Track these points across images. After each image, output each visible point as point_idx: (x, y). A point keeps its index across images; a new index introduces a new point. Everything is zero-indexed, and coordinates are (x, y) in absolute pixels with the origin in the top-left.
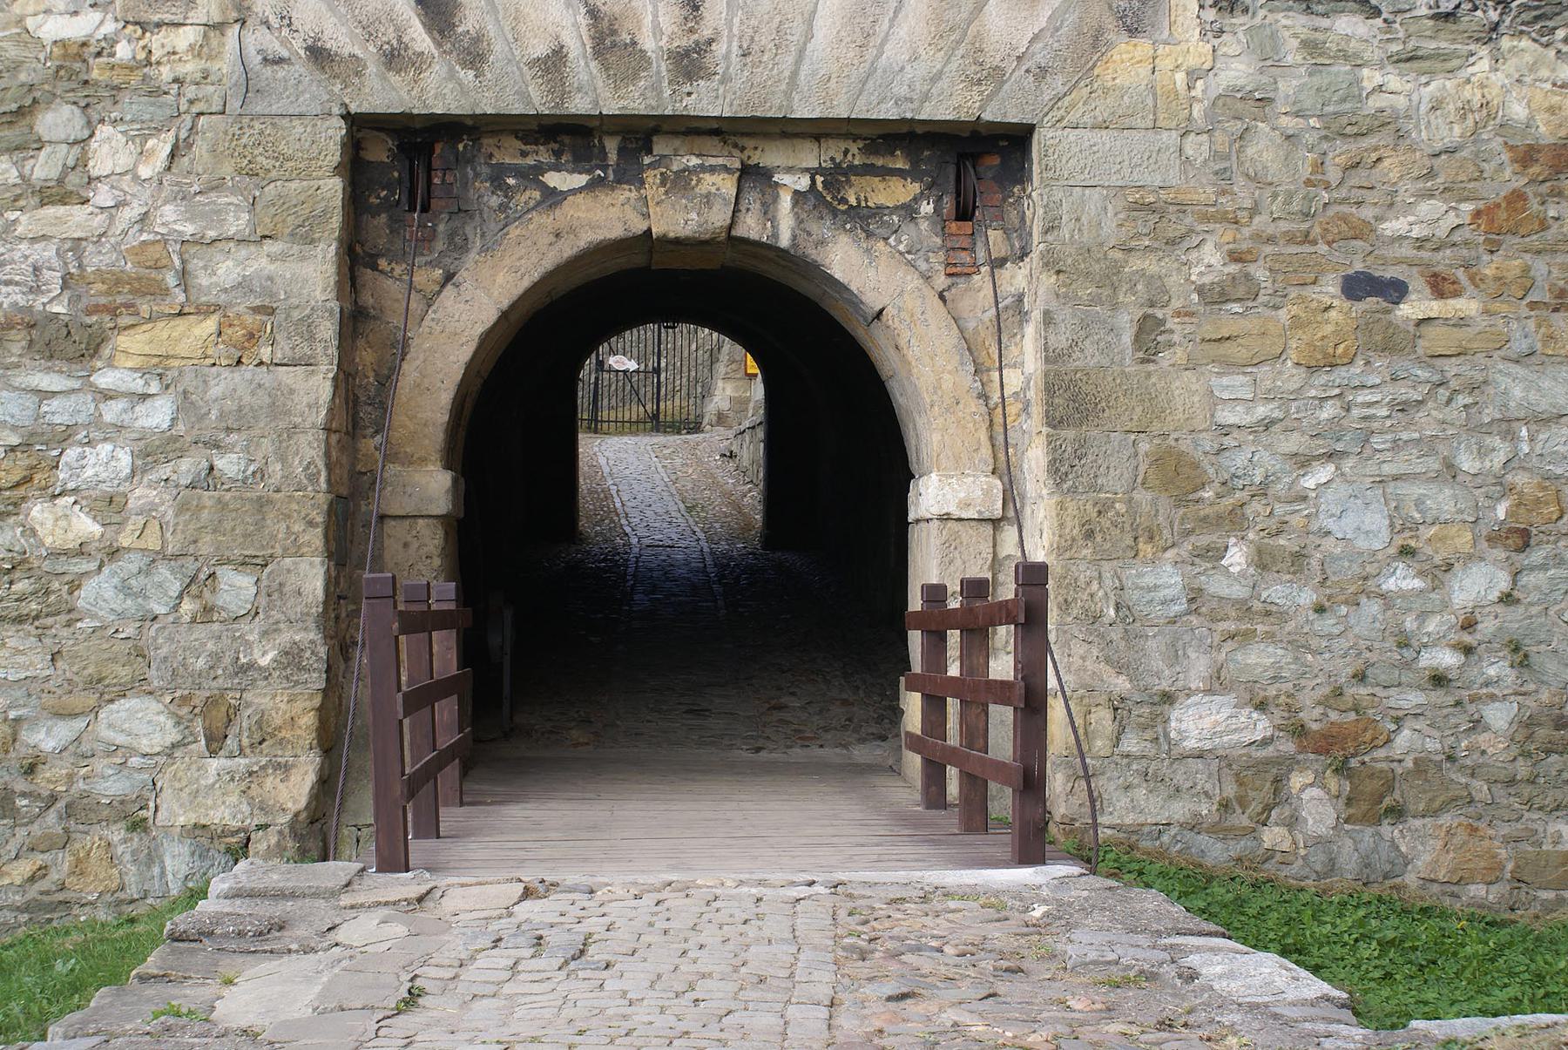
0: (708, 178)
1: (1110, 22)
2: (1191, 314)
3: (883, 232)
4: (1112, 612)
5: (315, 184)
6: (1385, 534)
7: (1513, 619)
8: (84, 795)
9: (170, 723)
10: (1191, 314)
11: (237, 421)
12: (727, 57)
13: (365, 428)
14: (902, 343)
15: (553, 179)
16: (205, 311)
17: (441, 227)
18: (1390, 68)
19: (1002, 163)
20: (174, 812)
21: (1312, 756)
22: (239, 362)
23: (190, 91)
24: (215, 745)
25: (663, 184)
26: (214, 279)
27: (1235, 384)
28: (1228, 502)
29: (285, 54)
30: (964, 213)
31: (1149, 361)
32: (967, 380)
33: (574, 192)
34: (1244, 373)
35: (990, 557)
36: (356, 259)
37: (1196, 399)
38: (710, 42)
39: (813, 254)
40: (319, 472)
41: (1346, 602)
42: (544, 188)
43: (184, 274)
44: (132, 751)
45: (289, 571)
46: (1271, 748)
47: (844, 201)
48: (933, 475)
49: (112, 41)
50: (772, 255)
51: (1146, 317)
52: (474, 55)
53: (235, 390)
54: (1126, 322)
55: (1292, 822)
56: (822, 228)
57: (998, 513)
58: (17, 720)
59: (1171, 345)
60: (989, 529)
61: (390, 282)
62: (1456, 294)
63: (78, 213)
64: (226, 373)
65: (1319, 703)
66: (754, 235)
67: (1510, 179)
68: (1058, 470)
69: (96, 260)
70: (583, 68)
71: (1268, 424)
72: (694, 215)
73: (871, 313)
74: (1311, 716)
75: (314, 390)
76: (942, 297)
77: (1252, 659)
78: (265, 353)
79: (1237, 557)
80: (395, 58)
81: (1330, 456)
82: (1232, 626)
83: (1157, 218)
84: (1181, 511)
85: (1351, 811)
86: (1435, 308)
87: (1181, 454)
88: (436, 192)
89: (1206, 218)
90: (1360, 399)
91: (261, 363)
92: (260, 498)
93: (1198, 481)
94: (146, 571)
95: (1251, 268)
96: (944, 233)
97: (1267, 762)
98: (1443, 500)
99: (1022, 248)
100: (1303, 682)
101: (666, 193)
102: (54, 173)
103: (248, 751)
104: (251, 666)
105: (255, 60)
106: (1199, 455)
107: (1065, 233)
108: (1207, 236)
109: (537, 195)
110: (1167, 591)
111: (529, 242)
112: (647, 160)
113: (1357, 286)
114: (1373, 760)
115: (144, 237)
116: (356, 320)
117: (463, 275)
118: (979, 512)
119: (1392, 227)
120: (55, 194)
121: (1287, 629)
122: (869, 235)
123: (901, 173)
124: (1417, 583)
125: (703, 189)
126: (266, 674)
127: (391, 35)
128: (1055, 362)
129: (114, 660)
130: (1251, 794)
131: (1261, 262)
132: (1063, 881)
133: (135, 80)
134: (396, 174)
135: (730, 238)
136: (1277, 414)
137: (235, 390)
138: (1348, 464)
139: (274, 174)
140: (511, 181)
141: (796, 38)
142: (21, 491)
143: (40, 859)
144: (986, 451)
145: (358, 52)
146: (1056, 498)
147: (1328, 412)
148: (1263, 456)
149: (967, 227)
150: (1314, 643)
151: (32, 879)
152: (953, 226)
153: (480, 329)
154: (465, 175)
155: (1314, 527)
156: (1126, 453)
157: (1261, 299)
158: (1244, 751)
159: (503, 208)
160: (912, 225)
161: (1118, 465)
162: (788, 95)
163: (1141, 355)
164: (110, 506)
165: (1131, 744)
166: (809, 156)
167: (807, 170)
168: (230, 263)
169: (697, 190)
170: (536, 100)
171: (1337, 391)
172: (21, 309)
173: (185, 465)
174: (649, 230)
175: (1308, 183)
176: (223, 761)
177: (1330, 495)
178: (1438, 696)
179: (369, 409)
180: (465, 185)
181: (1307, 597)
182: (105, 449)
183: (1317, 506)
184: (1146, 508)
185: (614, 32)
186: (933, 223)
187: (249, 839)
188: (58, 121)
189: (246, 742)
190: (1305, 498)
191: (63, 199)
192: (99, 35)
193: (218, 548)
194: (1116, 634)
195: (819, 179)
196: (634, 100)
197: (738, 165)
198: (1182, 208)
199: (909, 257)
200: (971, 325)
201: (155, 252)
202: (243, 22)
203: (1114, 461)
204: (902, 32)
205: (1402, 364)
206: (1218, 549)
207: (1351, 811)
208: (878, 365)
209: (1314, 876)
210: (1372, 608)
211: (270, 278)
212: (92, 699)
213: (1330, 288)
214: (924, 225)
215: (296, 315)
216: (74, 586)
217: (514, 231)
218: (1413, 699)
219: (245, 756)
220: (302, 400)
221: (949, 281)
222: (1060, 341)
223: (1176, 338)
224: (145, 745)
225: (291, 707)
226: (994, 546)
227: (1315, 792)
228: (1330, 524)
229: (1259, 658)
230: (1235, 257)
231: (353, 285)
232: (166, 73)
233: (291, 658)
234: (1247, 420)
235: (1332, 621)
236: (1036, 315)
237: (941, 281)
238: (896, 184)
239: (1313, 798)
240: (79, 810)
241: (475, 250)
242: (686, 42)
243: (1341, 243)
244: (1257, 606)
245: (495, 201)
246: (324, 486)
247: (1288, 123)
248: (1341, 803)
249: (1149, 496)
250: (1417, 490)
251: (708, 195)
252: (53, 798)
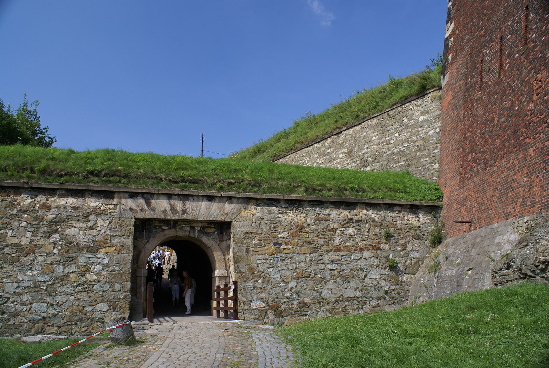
7: (297, 289)
8: (94, 318)
15: (163, 227)
23: (112, 214)
27: (260, 257)
36: (135, 239)
43: (111, 240)
44: (101, 311)
54: (245, 248)
55: (268, 318)
63: (95, 231)
67: (295, 229)
69: (97, 238)
70: (169, 212)
74: (270, 304)
75: (129, 258)
78: (122, 252)
79: (260, 281)
80: (142, 210)
81: (272, 267)
83: (249, 235)
86: (286, 247)
98: (288, 273)
105: (122, 210)
116: (135, 247)
119: (281, 235)
120: (92, 228)
126: (122, 299)
133: (104, 212)
135: (189, 236)
143: (87, 328)
151: (86, 331)
164: (99, 274)
165: (246, 308)
166: (200, 225)
170: (162, 216)
173: (110, 268)
178: (287, 300)
181: (269, 287)
188: (92, 218)
191: (93, 229)
196: (176, 217)
198: (252, 233)
205: (281, 254)
210: (279, 288)
213: (272, 244)
216: (93, 286)
217: (158, 235)
220: (128, 259)
224: (103, 310)
225: (125, 304)
229: (263, 295)
232: (109, 211)
233: (126, 297)
237: (218, 243)
240: (93, 320)
247: (266, 222)
252: (89, 318)
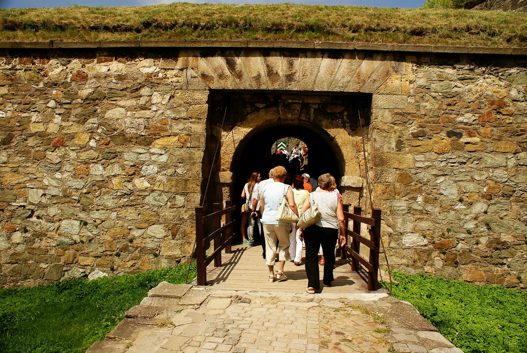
0: (294, 105)
1: (391, 70)
6: (457, 195)
7: (487, 217)
9: (164, 231)
10: (410, 140)
11: (182, 161)
12: (299, 76)
16: (175, 135)
17: (232, 116)
18: (459, 81)
20: (165, 252)
29: (196, 76)
38: (295, 73)
49: (158, 72)
52: (239, 76)
58: (130, 229)
59: (404, 147)
62: (475, 136)
63: (148, 112)
75: (199, 155)
77: (423, 225)
78: (189, 145)
79: (420, 199)
80: (221, 76)
82: (419, 216)
86: (469, 140)
90: (451, 161)
91: (188, 147)
94: (160, 195)
98: (471, 187)
102: (144, 103)
104: (183, 218)
112: (280, 101)
113: (450, 134)
115: (163, 117)
120: (144, 108)
124: (464, 207)
127: (220, 71)
128: (376, 151)
129: (152, 216)
132: (382, 299)
136: (430, 164)
141: (316, 72)
142: (133, 176)
143: (134, 261)
145: (212, 75)
157: (427, 136)
161: (391, 177)
162: (313, 86)
164: (152, 180)
165: (393, 245)
172: (135, 134)
173: (169, 170)
176: (176, 241)
182: (152, 166)
185: (272, 71)
192: (155, 71)
197: (301, 102)
201: (165, 121)
202: (187, 68)
204: (341, 71)
205: (460, 153)
212: (147, 225)
213: (443, 134)
215: (196, 136)
216: (144, 198)
218: (463, 236)
224: (158, 236)
229: (424, 225)
231: (211, 129)
234: (423, 166)
240: (143, 250)
242: (290, 73)
250: (464, 184)
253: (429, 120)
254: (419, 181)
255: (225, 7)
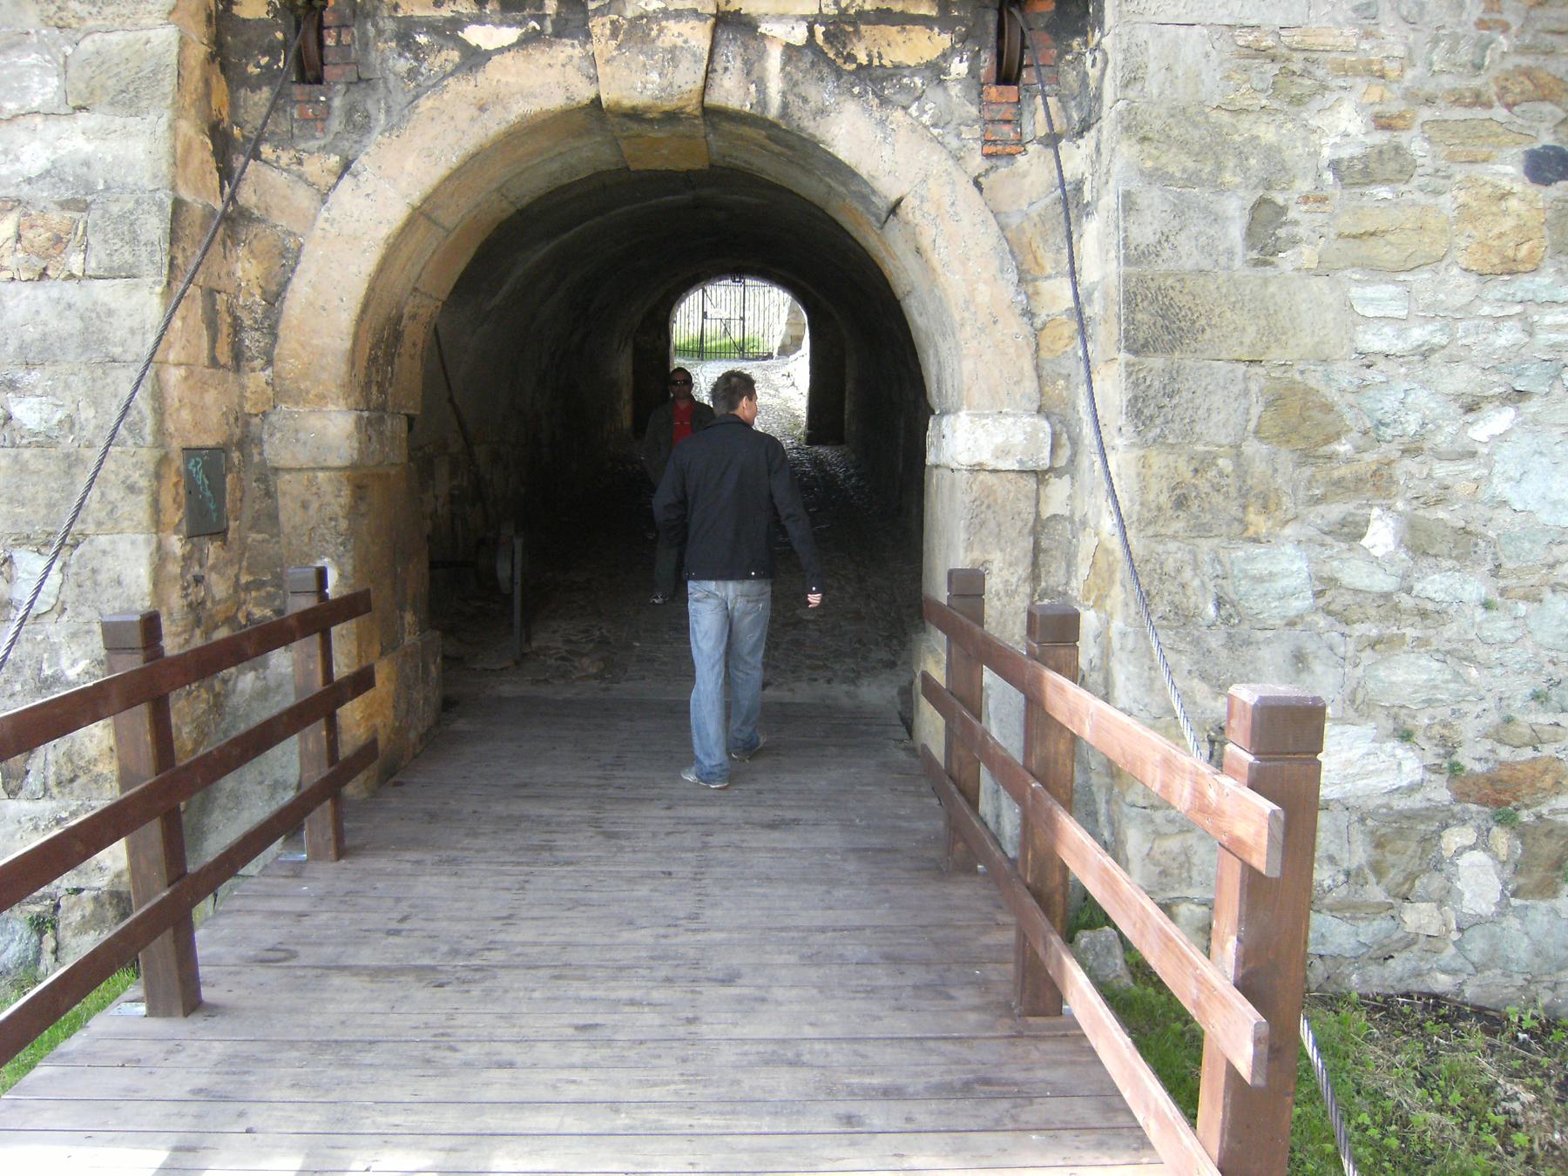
0: (672, 26)
2: (1323, 200)
3: (902, 98)
4: (1211, 610)
5: (143, 35)
13: (253, 359)
14: (925, 242)
15: (475, 35)
17: (337, 102)
19: (1058, 8)
21: (1473, 807)
22: (43, 274)
24: (13, 784)
25: (614, 35)
26: (18, 166)
27: (1377, 297)
28: (1371, 457)
30: (1007, 75)
31: (1265, 263)
32: (1007, 290)
33: (501, 51)
34: (1395, 282)
35: (1031, 518)
37: (1329, 316)
39: (810, 126)
40: (142, 420)
41: (1526, 598)
42: (464, 46)
45: (104, 552)
46: (1418, 796)
47: (851, 58)
48: (962, 414)
50: (759, 135)
51: (1262, 202)
53: (38, 312)
54: (1235, 208)
56: (820, 93)
57: (1044, 461)
59: (1294, 242)
60: (1031, 483)
61: (275, 174)
64: (27, 290)
65: (1486, 736)
66: (734, 103)
68: (1140, 412)
71: (1425, 353)
72: (654, 76)
73: (882, 206)
74: (1471, 758)
76: (977, 184)
77: (1399, 676)
78: (75, 262)
79: (1381, 535)
84: (1307, 471)
85: (1521, 880)
87: (1309, 391)
88: (330, 57)
89: (1344, 70)
90: (1549, 320)
91: (72, 276)
92: (67, 456)
93: (1331, 430)
95: (1403, 138)
96: (981, 101)
97: (1412, 816)
99: (1082, 120)
100: (1465, 707)
101: (619, 47)
103: (55, 791)
106: (1333, 395)
107: (1153, 88)
108: (1343, 94)
109: (455, 56)
110: (1285, 582)
111: (445, 118)
114: (1552, 811)
117: (363, 162)
118: (1021, 462)
121: (1447, 634)
122: (884, 102)
123: (925, 21)
125: (666, 41)
128: (1138, 262)
130: (1391, 858)
131: (1416, 130)
134: (279, 35)
136: (1440, 339)
137: (38, 312)
138: (1532, 407)
139: (90, 23)
140: (422, 39)
144: (1030, 385)
146: (1138, 452)
147: (1508, 336)
148: (1421, 397)
149: (1011, 92)
150: (1481, 652)
152: (993, 92)
153: (386, 231)
154: (364, 33)
155: (1484, 495)
156: (1236, 389)
158: (1384, 800)
159: (413, 74)
160: (939, 91)
161: (1224, 409)
163: (1254, 254)
167: (804, 18)
168: (37, 145)
169: (659, 43)
171: (1518, 309)
174: (598, 98)
175: (1481, 24)
177: (1506, 450)
179: (257, 335)
180: (365, 46)
183: (1490, 465)
184: (1259, 467)
186: (967, 89)
187: (57, 907)
189: (51, 781)
190: (1473, 454)
193: (15, 523)
194: (1215, 641)
195: (819, 30)
199: (936, 132)
200: (1014, 221)
203: (1217, 400)
206: (1356, 524)
207: (1521, 880)
208: (893, 280)
209: (1470, 969)
211: (86, 164)
213: (1508, 170)
214: (955, 90)
217: (425, 104)
219: (52, 797)
221: (987, 164)
222: (1144, 233)
223: (1301, 231)
226: (1038, 503)
227: (1478, 856)
228: (1503, 489)
230: (1383, 123)
234: (1399, 346)
235: (1503, 625)
236: (1109, 201)
237: (977, 163)
238: (919, 34)
239: (1472, 865)
241: (378, 130)
243: (1525, 106)
244: (1406, 601)
245: (402, 65)
246: (150, 439)
248: (1509, 868)
249: (1264, 448)
251: (673, 50)
253: (1430, 87)
254: (1373, 434)
255: (941, 300)
